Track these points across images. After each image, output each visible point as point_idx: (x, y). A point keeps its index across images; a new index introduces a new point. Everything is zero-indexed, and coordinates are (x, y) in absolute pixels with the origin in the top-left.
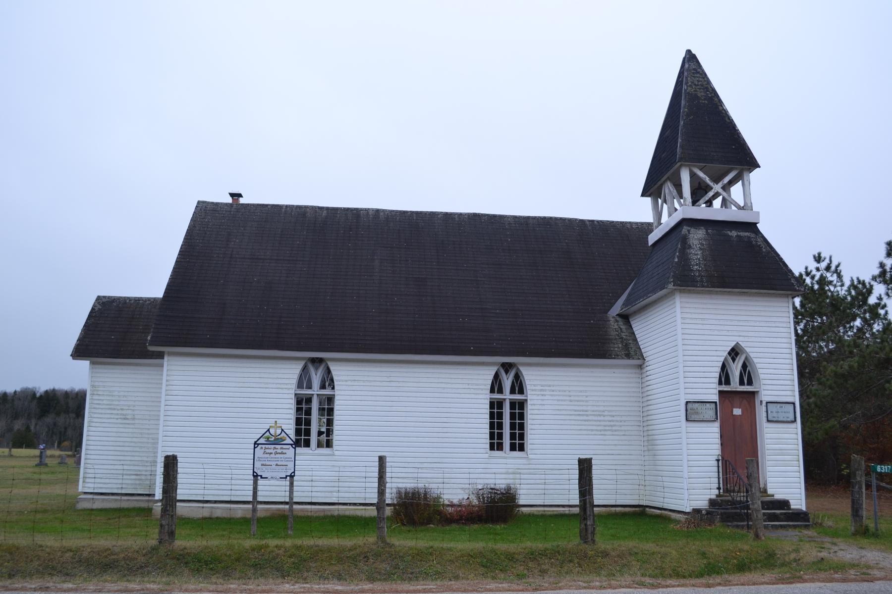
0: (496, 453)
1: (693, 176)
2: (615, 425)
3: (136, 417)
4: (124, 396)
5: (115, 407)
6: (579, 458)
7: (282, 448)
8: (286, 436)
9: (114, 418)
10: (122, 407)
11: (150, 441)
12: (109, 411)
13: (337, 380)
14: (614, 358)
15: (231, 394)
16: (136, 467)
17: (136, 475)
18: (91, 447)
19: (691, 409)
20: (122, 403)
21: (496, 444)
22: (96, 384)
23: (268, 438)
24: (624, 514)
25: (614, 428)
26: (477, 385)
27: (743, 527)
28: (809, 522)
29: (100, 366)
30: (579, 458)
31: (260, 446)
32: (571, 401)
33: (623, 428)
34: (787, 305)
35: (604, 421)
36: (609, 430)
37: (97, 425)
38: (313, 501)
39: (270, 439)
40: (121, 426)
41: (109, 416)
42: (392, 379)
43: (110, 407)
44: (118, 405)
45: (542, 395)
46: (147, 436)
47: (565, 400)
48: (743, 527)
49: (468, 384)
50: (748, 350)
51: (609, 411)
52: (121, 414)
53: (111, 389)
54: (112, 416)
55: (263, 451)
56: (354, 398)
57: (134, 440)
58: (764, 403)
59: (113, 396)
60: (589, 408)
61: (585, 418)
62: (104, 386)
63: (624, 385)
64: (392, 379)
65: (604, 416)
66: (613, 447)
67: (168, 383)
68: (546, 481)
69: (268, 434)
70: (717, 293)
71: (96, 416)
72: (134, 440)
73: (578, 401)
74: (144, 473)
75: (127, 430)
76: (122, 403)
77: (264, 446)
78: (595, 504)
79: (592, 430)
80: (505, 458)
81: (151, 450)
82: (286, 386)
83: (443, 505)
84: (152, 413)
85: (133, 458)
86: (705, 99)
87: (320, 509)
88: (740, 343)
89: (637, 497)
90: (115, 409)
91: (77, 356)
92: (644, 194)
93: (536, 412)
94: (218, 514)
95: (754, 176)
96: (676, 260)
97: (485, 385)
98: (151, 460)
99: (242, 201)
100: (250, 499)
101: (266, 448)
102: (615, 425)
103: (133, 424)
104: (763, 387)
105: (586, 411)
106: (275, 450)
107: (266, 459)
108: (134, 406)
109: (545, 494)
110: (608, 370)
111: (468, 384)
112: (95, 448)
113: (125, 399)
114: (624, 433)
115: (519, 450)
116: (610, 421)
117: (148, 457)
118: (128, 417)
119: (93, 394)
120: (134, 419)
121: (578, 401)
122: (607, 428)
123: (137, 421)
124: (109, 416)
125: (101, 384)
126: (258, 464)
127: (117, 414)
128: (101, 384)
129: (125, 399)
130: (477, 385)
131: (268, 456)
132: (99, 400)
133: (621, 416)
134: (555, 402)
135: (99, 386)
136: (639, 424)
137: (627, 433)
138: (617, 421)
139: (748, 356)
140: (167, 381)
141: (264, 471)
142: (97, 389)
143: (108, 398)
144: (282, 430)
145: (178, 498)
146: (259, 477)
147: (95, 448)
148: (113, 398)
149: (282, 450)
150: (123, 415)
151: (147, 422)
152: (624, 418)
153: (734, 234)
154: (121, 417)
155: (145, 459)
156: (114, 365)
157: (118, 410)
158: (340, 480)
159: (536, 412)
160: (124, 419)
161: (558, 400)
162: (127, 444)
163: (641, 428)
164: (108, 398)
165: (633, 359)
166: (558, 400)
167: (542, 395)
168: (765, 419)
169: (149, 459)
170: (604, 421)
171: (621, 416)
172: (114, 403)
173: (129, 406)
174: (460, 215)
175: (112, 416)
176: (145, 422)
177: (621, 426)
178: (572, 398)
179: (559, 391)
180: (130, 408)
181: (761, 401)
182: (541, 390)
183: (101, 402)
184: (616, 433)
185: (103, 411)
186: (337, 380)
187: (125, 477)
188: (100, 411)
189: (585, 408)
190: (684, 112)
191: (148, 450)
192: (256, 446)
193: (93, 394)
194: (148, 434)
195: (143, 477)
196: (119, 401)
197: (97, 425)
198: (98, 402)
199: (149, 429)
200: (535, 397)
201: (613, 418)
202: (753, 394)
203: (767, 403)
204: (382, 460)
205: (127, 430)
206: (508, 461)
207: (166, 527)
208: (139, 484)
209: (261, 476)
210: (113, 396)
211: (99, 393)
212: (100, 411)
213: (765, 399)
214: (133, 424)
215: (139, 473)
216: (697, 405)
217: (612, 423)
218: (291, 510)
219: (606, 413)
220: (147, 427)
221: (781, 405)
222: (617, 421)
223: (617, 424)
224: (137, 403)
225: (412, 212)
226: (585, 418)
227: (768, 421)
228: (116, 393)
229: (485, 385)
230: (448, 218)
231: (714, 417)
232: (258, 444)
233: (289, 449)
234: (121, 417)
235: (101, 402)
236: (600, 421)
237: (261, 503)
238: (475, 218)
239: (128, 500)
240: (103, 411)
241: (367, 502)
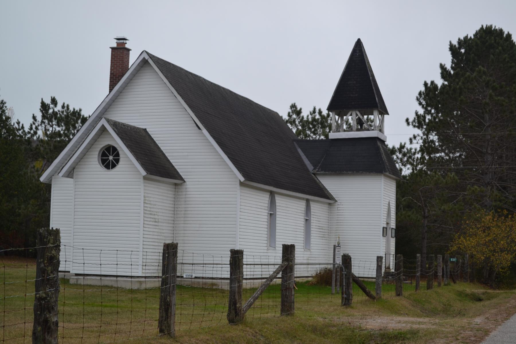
3: (160, 220)
95: (386, 116)
114: (325, 239)
123: (160, 224)
241: (255, 277)
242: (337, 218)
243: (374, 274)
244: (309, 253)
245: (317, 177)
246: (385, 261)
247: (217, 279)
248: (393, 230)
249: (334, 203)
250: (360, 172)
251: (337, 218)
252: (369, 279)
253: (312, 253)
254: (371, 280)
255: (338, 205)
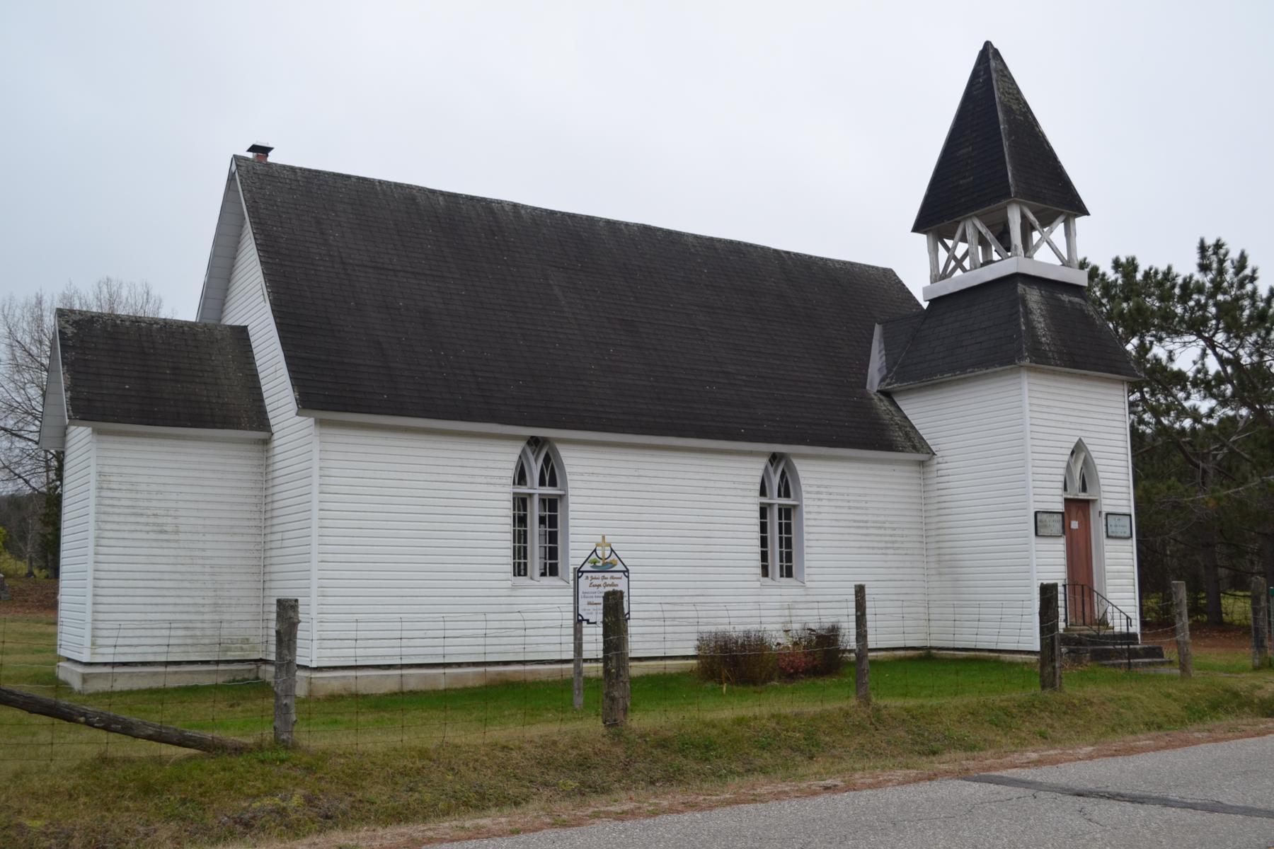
0: (521, 580)
1: (1024, 217)
2: (896, 542)
3: (182, 528)
4: (158, 492)
5: (142, 511)
6: (1042, 584)
7: (612, 578)
8: (617, 559)
9: (141, 531)
10: (155, 512)
11: (208, 569)
12: (132, 519)
13: (570, 473)
14: (902, 451)
15: (420, 493)
16: (185, 615)
17: (186, 628)
18: (103, 583)
19: (1041, 521)
20: (154, 504)
21: (520, 570)
22: (106, 469)
23: (595, 563)
24: (910, 659)
25: (896, 545)
26: (744, 483)
27: (1120, 665)
28: (1162, 657)
29: (111, 438)
30: (1042, 584)
31: (585, 574)
32: (850, 508)
33: (905, 545)
34: (1122, 393)
35: (885, 535)
36: (890, 548)
37: (112, 542)
38: (487, 660)
39: (597, 564)
40: (154, 544)
41: (133, 527)
42: (641, 472)
43: (135, 511)
44: (148, 508)
45: (819, 499)
46: (201, 561)
47: (843, 507)
48: (1120, 665)
49: (734, 482)
50: (1090, 448)
51: (891, 522)
52: (154, 524)
53: (134, 479)
54: (139, 528)
55: (588, 582)
56: (593, 500)
57: (180, 568)
58: (1103, 515)
59: (137, 491)
60: (870, 518)
61: (865, 531)
62: (121, 475)
63: (906, 487)
64: (641, 472)
65: (885, 528)
66: (894, 571)
67: (322, 473)
68: (662, 623)
69: (594, 556)
70: (1061, 374)
71: (108, 526)
72: (180, 568)
73: (857, 508)
74: (199, 625)
75: (165, 552)
76: (154, 504)
77: (589, 575)
78: (869, 647)
79: (873, 548)
80: (780, 587)
81: (210, 586)
82: (498, 481)
83: (844, 651)
84: (208, 522)
85: (178, 601)
86: (1020, 115)
87: (553, 669)
88: (1083, 439)
89: (923, 636)
90: (142, 515)
91: (80, 419)
92: (918, 228)
93: (813, 523)
94: (412, 685)
95: (1080, 222)
96: (1023, 328)
97: (754, 484)
98: (210, 602)
99: (272, 158)
100: (570, 656)
101: (592, 578)
102: (896, 542)
103: (177, 541)
104: (1103, 495)
105: (866, 522)
106: (605, 581)
107: (594, 595)
108: (176, 509)
109: (168, 645)
110: (886, 467)
111: (734, 482)
112: (111, 583)
113: (160, 497)
114: (905, 552)
115: (551, 575)
116: (891, 536)
117: (204, 598)
118: (165, 528)
119: (102, 488)
120: (177, 532)
121: (857, 508)
122: (889, 545)
123: (182, 536)
124: (133, 527)
125: (115, 470)
126: (582, 602)
127: (147, 524)
128: (115, 470)
129: (160, 497)
130: (744, 483)
131: (595, 589)
132: (112, 498)
133: (903, 529)
134: (834, 510)
135: (111, 474)
136: (921, 540)
137: (909, 552)
138: (899, 536)
139: (1088, 456)
140: (321, 468)
141: (591, 613)
142: (108, 478)
143: (129, 495)
144: (612, 550)
145: (632, 655)
146: (584, 624)
147: (111, 583)
148: (139, 496)
149: (613, 580)
150: (158, 525)
151: (201, 537)
152: (906, 532)
153: (1065, 298)
154: (155, 528)
155: (201, 601)
156: (139, 437)
157: (148, 516)
158: (122, 626)
159: (813, 523)
160: (161, 532)
161: (836, 507)
162: (166, 576)
163: (924, 546)
164: (129, 495)
165: (922, 453)
166: (836, 507)
167: (819, 499)
168: (1104, 534)
169: (206, 601)
170: (885, 535)
171: (903, 529)
172: (141, 504)
173: (167, 509)
174: (627, 225)
175: (139, 528)
176: (195, 537)
177: (902, 542)
178: (851, 504)
179: (837, 494)
180: (170, 513)
181: (1100, 512)
182: (818, 493)
183: (115, 502)
184: (897, 552)
185: (122, 519)
186: (570, 473)
187: (667, 623)
188: (116, 518)
189: (865, 518)
190: (1004, 128)
191: (203, 586)
192: (580, 574)
193: (102, 488)
194: (203, 558)
195: (198, 633)
196: (149, 500)
197: (112, 542)
198: (111, 502)
199: (203, 550)
200: (810, 502)
201: (894, 532)
202: (1087, 502)
203: (1107, 514)
204: (860, 591)
205: (165, 552)
206: (784, 591)
207: (621, 700)
208: (192, 645)
209: (588, 621)
210: (137, 491)
211: (113, 486)
212: (116, 518)
213: (1105, 509)
214: (177, 541)
215: (190, 625)
216: (1045, 515)
217: (894, 539)
218: (579, 672)
219: (887, 525)
220: (200, 545)
221: (1121, 517)
222: (899, 536)
223: (898, 539)
224: (181, 505)
225: (563, 214)
226: (865, 531)
227: (1108, 537)
228: (143, 487)
229: (754, 484)
230: (613, 227)
231: (1128, 532)
232: (583, 572)
233: (620, 578)
234: (155, 528)
235: (115, 502)
236: (881, 535)
237: (585, 661)
238: (646, 230)
239: (176, 673)
240: (122, 519)
241: (447, 660)
242: (939, 496)
243: (1033, 642)
244: (801, 591)
245: (899, 403)
246: (1063, 605)
247: (544, 664)
248: (1109, 517)
249: (930, 459)
250: (968, 370)
251: (939, 496)
252: (1000, 655)
253: (810, 591)
254: (1018, 657)
255: (938, 463)
